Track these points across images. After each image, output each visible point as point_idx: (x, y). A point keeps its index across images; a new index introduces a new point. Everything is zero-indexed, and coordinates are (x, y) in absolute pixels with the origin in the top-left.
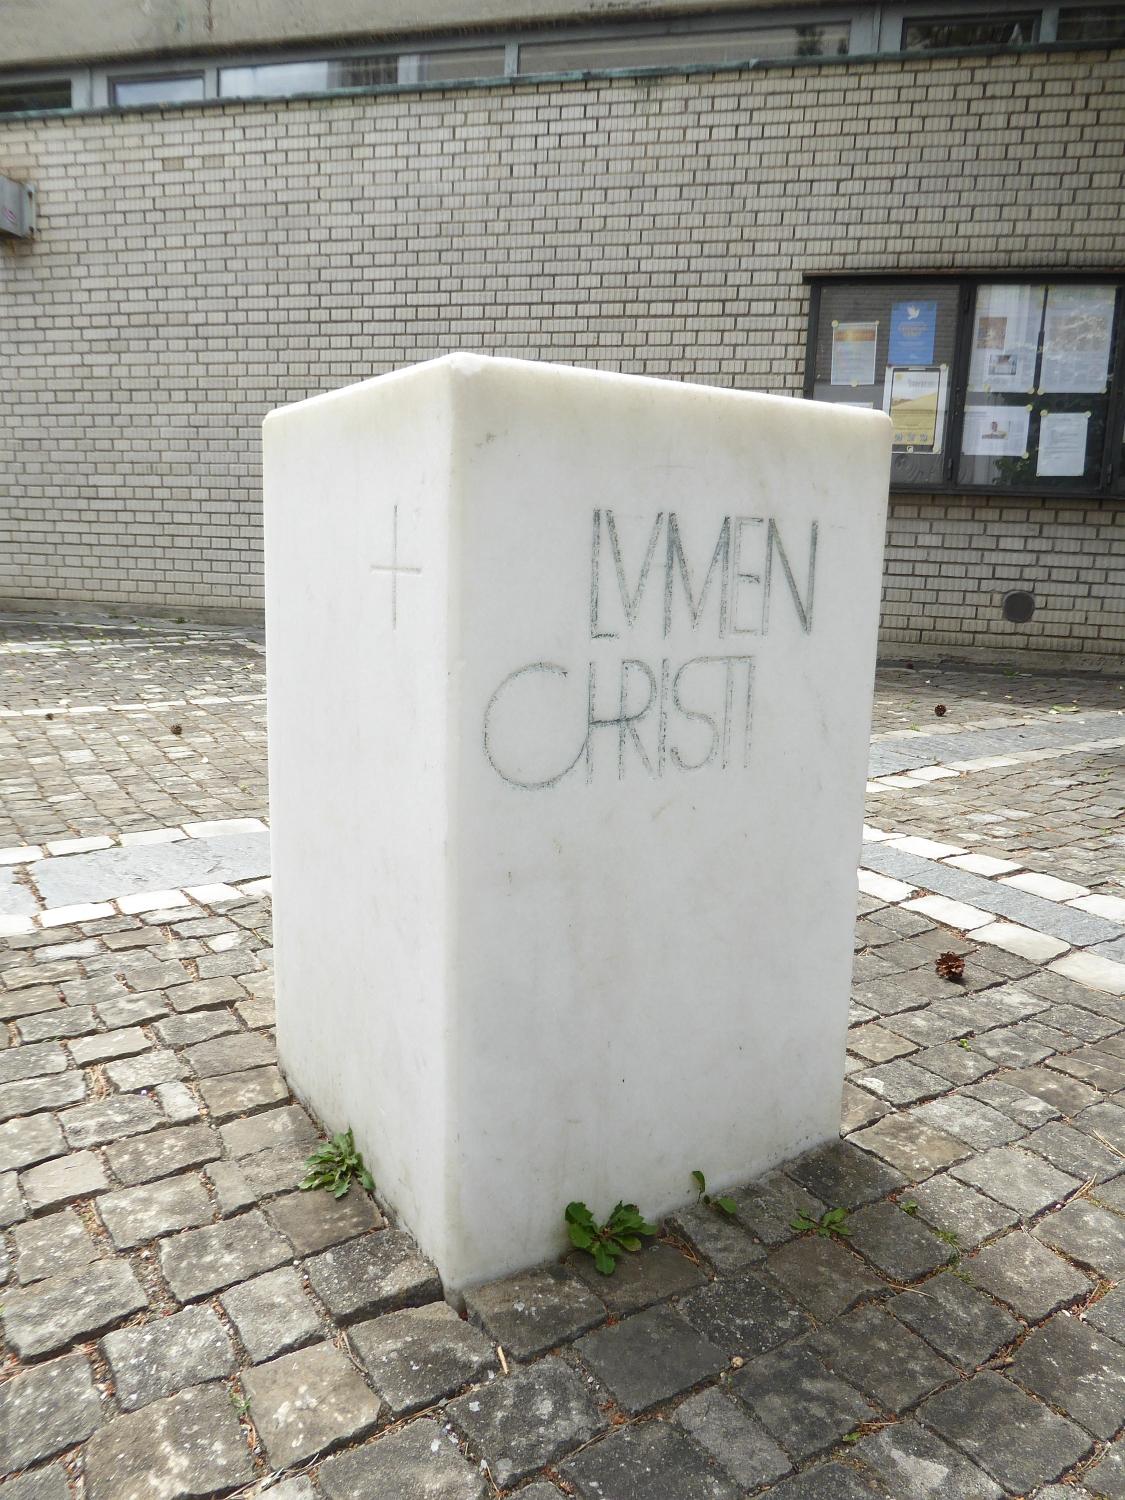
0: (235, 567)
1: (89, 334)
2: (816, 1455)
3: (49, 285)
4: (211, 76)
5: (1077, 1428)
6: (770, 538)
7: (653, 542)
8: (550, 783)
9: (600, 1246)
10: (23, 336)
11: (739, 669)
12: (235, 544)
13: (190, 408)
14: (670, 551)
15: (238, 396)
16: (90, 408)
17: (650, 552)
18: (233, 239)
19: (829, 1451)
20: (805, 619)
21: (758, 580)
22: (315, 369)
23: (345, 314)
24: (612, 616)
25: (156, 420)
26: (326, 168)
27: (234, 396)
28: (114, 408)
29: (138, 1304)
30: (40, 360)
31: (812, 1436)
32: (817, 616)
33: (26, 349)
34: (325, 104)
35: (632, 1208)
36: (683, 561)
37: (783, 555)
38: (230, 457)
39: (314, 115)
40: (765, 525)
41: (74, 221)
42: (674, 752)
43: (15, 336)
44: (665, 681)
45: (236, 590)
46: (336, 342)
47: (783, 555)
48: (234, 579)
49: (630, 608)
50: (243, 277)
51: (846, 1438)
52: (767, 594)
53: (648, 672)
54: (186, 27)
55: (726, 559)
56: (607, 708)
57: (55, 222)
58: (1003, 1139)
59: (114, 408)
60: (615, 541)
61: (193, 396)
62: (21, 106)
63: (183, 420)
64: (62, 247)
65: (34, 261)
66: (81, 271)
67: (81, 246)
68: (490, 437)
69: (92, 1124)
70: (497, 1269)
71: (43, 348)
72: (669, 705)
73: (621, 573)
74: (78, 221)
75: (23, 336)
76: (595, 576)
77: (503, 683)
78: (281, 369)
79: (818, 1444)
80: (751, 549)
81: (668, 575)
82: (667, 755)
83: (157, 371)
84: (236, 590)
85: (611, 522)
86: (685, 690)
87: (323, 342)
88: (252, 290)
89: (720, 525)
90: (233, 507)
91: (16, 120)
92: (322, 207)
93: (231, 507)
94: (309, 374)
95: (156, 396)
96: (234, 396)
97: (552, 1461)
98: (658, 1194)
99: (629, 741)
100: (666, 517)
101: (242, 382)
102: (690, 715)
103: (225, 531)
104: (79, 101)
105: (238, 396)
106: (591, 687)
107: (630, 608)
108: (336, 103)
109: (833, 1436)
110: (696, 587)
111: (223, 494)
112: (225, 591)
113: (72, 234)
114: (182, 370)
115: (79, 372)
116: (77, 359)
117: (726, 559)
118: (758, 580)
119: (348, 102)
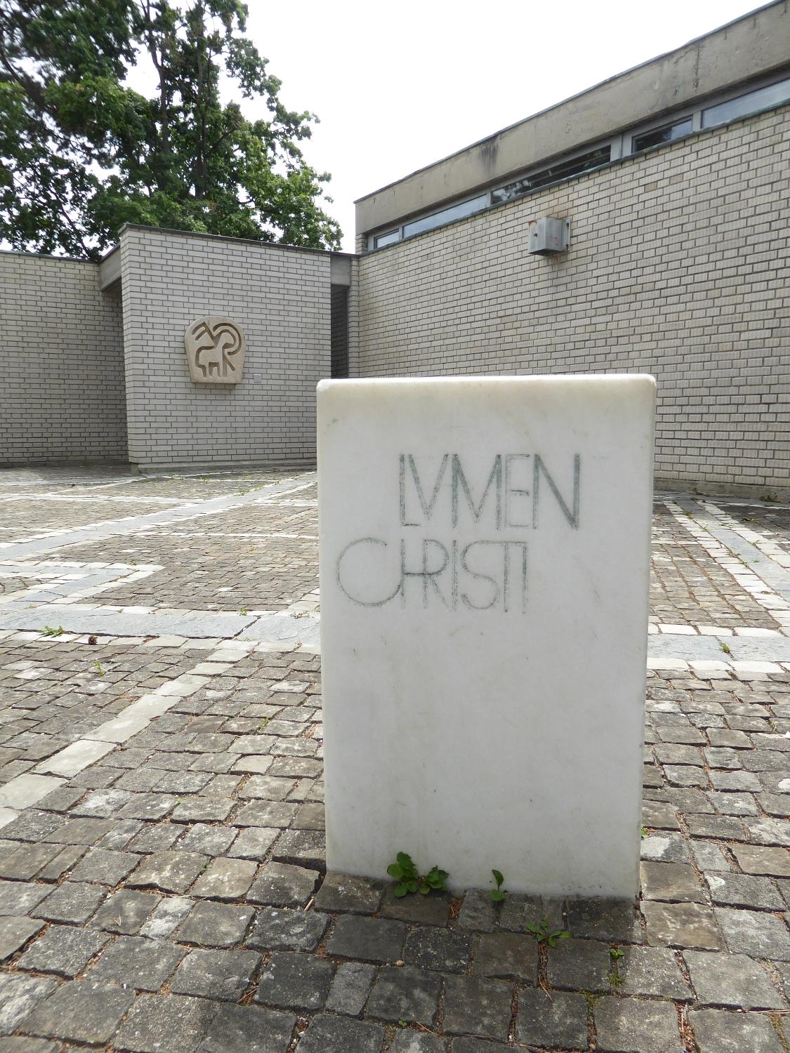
0: (677, 451)
1: (595, 304)
2: (379, 1020)
3: (575, 278)
4: (697, 118)
5: (56, 859)
6: (536, 467)
7: (442, 471)
8: (380, 604)
9: (415, 889)
10: (560, 310)
11: (515, 553)
12: (678, 435)
13: (653, 345)
14: (455, 478)
15: (685, 333)
16: (593, 351)
17: (440, 477)
18: (687, 227)
19: (387, 1022)
20: (573, 520)
21: (527, 493)
22: (740, 308)
23: (764, 266)
24: (415, 513)
25: (632, 355)
26: (753, 165)
27: (682, 334)
28: (607, 350)
29: (219, 818)
30: (567, 324)
31: (386, 1011)
32: (582, 517)
33: (560, 318)
34: (754, 120)
35: (443, 874)
36: (465, 483)
37: (549, 478)
38: (678, 375)
39: (747, 130)
40: (531, 460)
41: (592, 235)
42: (464, 596)
43: (555, 311)
44: (459, 553)
45: (677, 467)
46: (756, 287)
47: (549, 478)
48: (676, 459)
49: (428, 510)
50: (692, 252)
51: (400, 1022)
52: (535, 503)
53: (443, 548)
54: (681, 90)
55: (499, 481)
56: (414, 564)
57: (581, 238)
58: (764, 955)
59: (607, 350)
60: (414, 471)
61: (656, 336)
62: (582, 168)
63: (648, 353)
64: (583, 253)
65: (568, 264)
66: (593, 266)
67: (594, 251)
68: (334, 421)
69: (284, 746)
70: (352, 870)
71: (570, 316)
72: (459, 568)
73: (419, 489)
74: (593, 235)
75: (560, 310)
76: (402, 490)
77: (347, 548)
78: (715, 311)
79: (383, 1015)
80: (521, 474)
81: (454, 490)
82: (459, 598)
83: (633, 323)
84: (677, 467)
85: (412, 461)
86: (469, 558)
87: (747, 288)
88: (699, 260)
89: (493, 460)
90: (678, 410)
91: (563, 183)
92: (751, 193)
93: (677, 410)
94: (735, 313)
95: (633, 339)
96: (682, 334)
97: (273, 949)
98: (468, 874)
99: (431, 588)
100: (451, 458)
101: (688, 324)
102: (476, 576)
103: (671, 427)
104: (614, 156)
105: (685, 333)
106: (402, 553)
107: (428, 510)
108: (763, 117)
109: (394, 1017)
110: (476, 496)
111: (671, 401)
112: (669, 467)
113: (589, 244)
114: (650, 320)
115: (589, 329)
116: (587, 321)
117: (499, 481)
118: (527, 493)
119: (772, 114)
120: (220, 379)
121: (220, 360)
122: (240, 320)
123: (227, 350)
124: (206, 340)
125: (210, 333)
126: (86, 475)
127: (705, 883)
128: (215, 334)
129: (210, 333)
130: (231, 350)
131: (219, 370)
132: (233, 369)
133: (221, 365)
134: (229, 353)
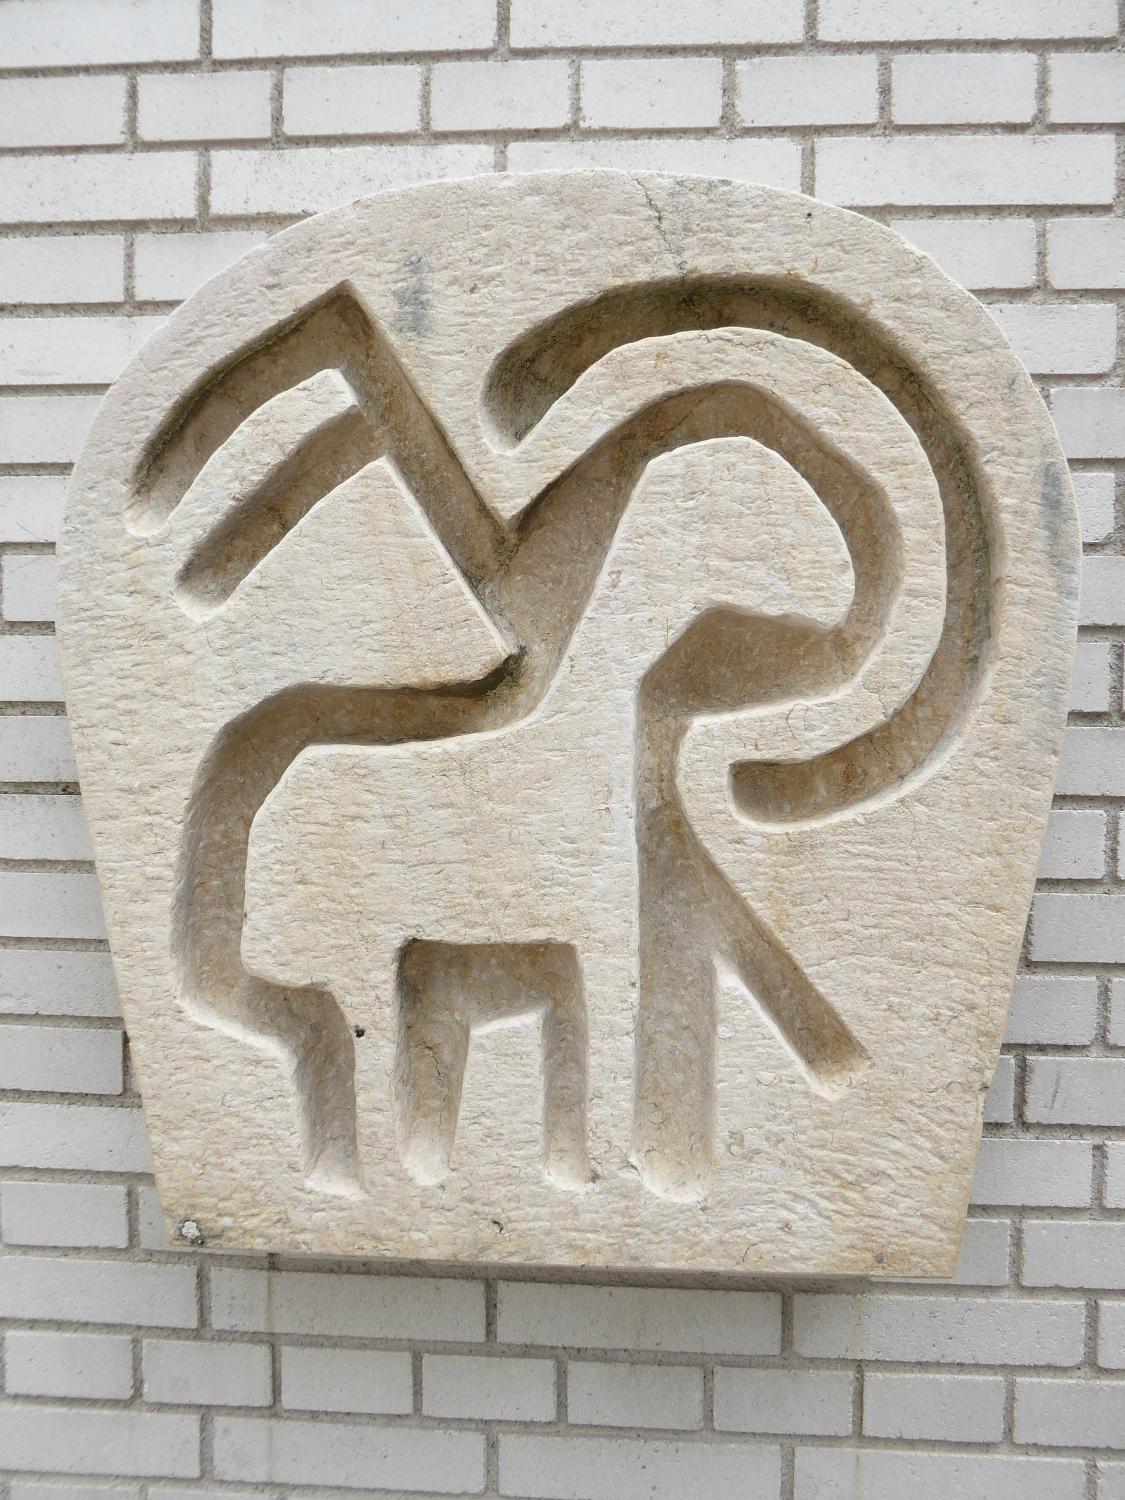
120: (567, 1206)
121: (596, 904)
122: (1004, 251)
123: (717, 738)
124: (366, 583)
125: (438, 477)
126: (771, 276)
127: (684, 1094)
128: (510, 470)
129: (438, 477)
130: (807, 722)
131: (565, 1042)
132: (821, 1037)
133: (610, 982)
134: (763, 784)
